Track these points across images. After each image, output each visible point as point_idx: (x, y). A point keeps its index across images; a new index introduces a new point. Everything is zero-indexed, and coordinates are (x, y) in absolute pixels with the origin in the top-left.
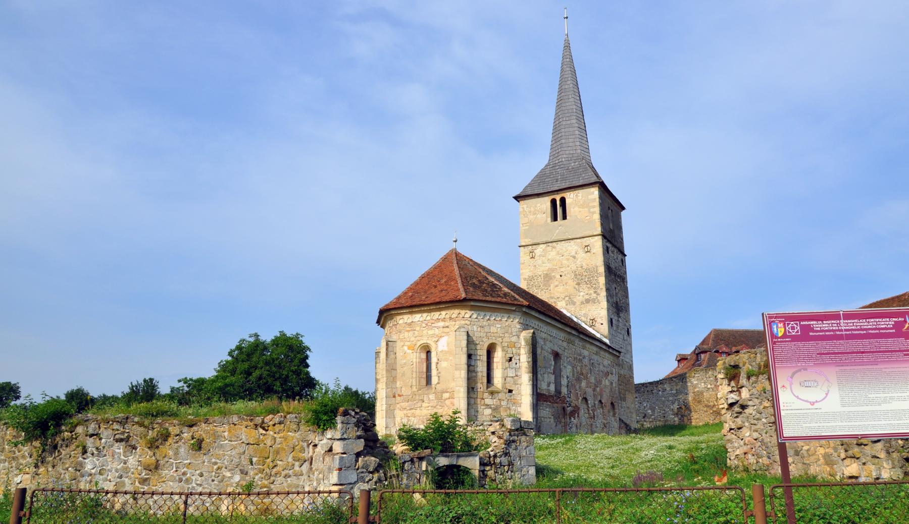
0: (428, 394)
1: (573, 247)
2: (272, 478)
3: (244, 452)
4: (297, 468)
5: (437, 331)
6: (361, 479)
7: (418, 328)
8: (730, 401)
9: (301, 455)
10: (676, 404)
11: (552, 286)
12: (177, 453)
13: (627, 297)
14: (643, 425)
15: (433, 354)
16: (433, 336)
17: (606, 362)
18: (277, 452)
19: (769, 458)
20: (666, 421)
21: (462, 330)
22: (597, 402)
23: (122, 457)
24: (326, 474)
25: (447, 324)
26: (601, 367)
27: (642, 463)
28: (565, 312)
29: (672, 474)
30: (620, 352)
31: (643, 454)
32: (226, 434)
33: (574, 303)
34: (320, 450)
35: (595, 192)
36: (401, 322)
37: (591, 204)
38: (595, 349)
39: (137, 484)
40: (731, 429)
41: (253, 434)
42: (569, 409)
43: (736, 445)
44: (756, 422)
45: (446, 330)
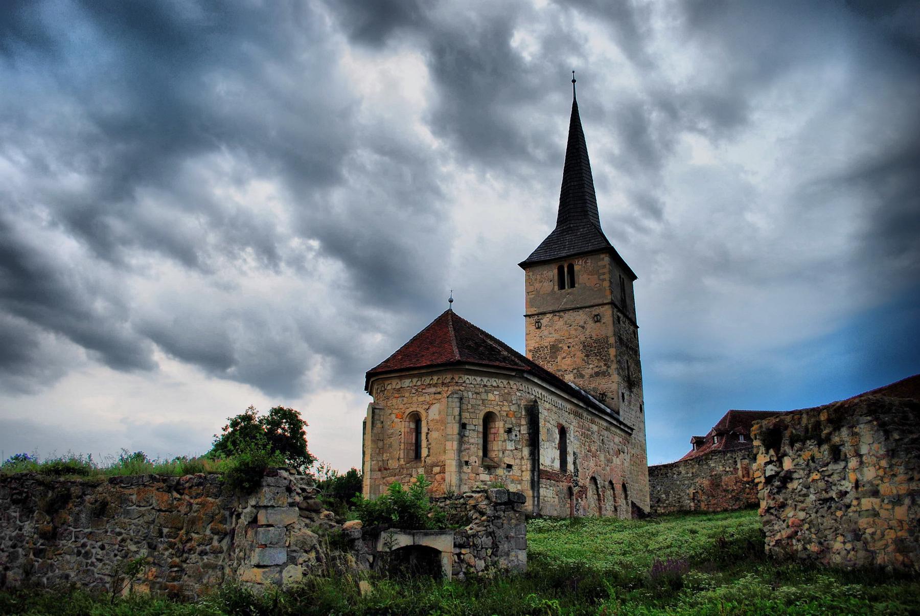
0: (417, 468)
2: (185, 555)
3: (153, 521)
4: (215, 543)
5: (428, 398)
6: (292, 560)
7: (407, 395)
8: (768, 474)
9: (222, 527)
10: (693, 487)
11: (559, 358)
12: (77, 520)
13: (640, 371)
14: (656, 511)
15: (424, 424)
16: (423, 403)
17: (617, 439)
18: (193, 522)
19: (820, 543)
20: (682, 506)
21: (455, 396)
22: (607, 483)
23: (18, 522)
24: (248, 551)
25: (439, 390)
26: (612, 444)
27: (660, 549)
28: (573, 385)
29: (697, 562)
30: (632, 430)
31: (660, 539)
32: (134, 497)
33: (582, 376)
34: (244, 520)
35: (606, 259)
36: (389, 387)
37: (601, 271)
38: (605, 424)
39: (31, 556)
40: (770, 508)
41: (165, 498)
42: (576, 490)
43: (776, 527)
44: (801, 498)
45: (438, 396)
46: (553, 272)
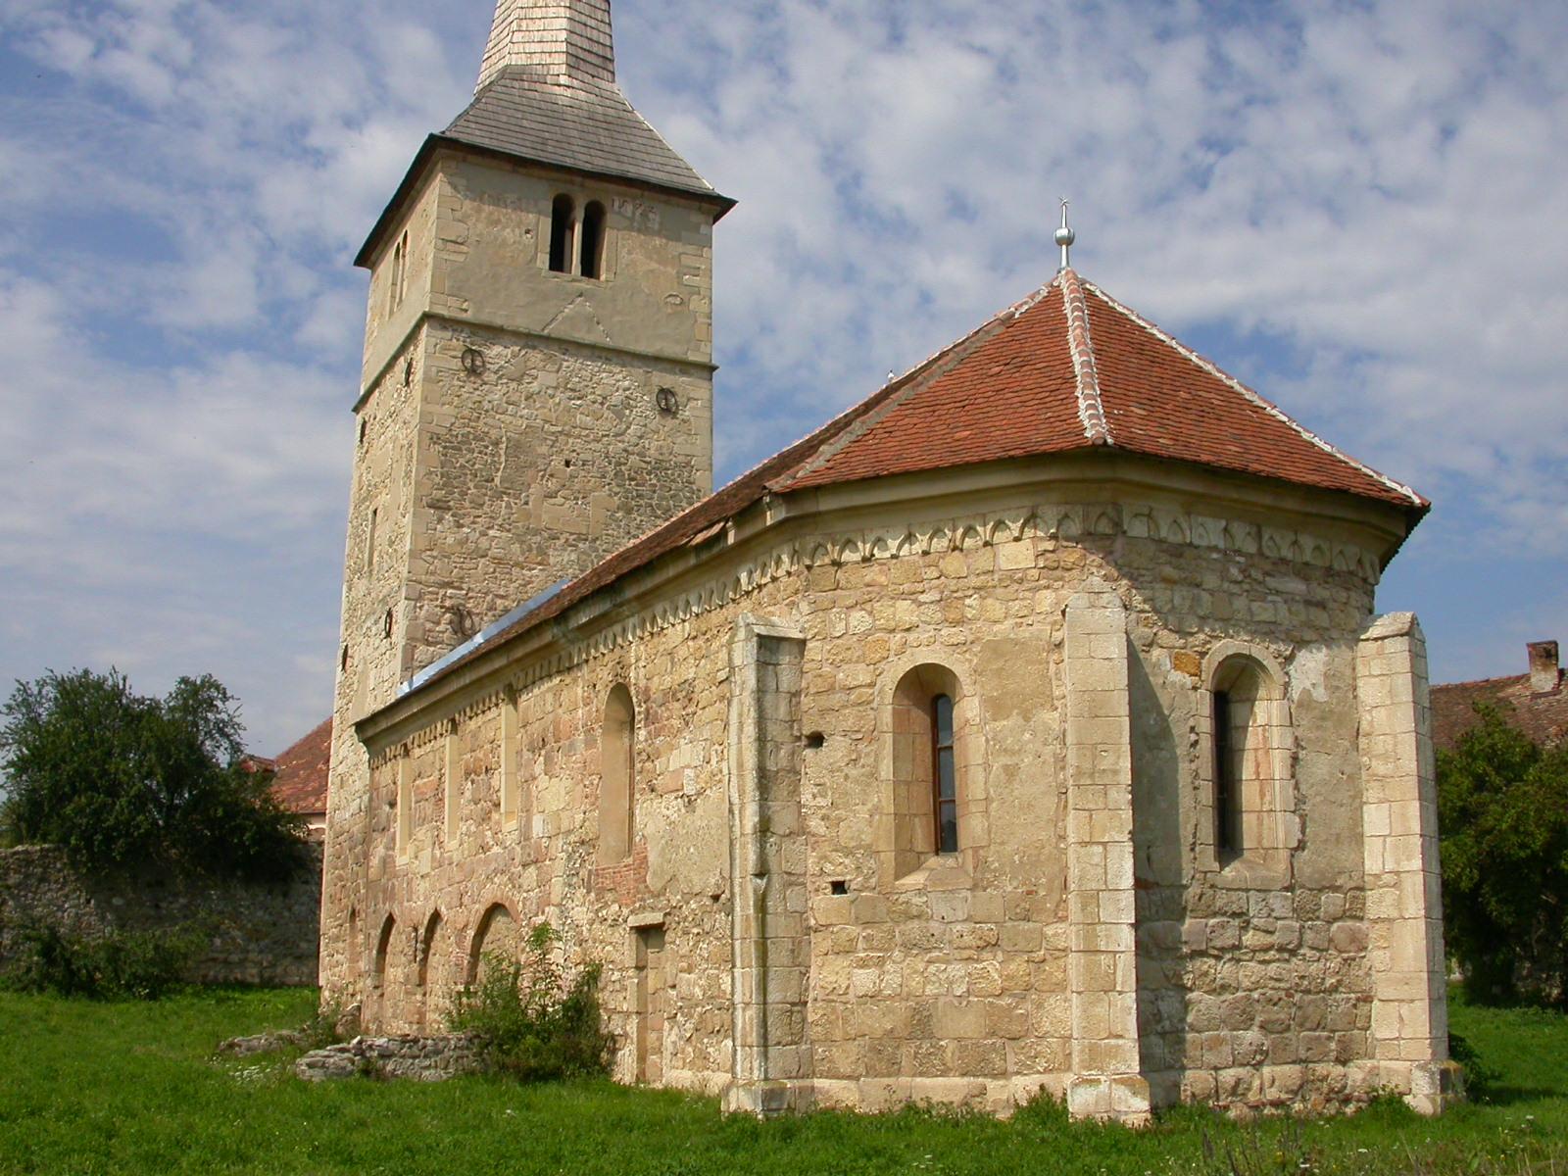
1: (618, 380)
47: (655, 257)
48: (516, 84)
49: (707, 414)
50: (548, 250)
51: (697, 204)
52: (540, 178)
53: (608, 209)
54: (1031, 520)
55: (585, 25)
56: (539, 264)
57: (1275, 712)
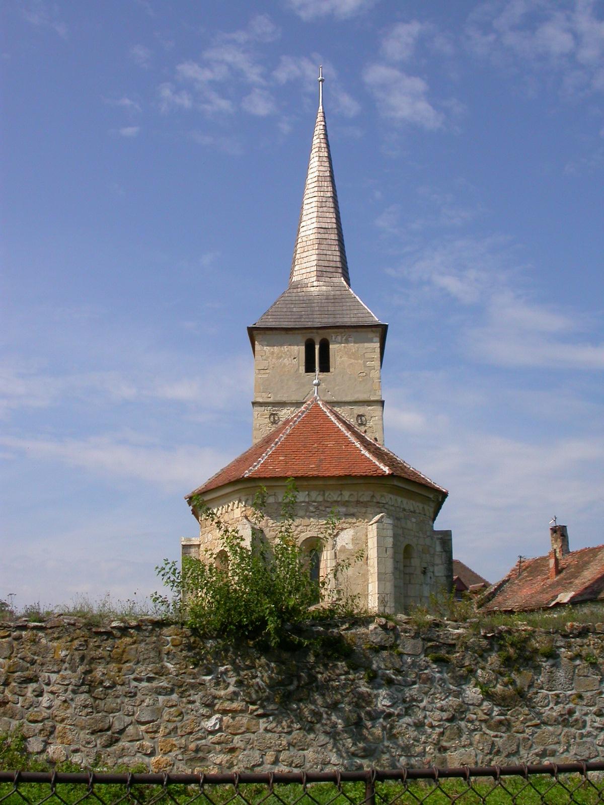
46: (300, 350)
47: (353, 357)
48: (295, 291)
49: (381, 422)
50: (304, 364)
51: (370, 329)
52: (298, 334)
53: (330, 341)
54: (240, 501)
55: (326, 255)
56: (301, 372)
57: (329, 554)
